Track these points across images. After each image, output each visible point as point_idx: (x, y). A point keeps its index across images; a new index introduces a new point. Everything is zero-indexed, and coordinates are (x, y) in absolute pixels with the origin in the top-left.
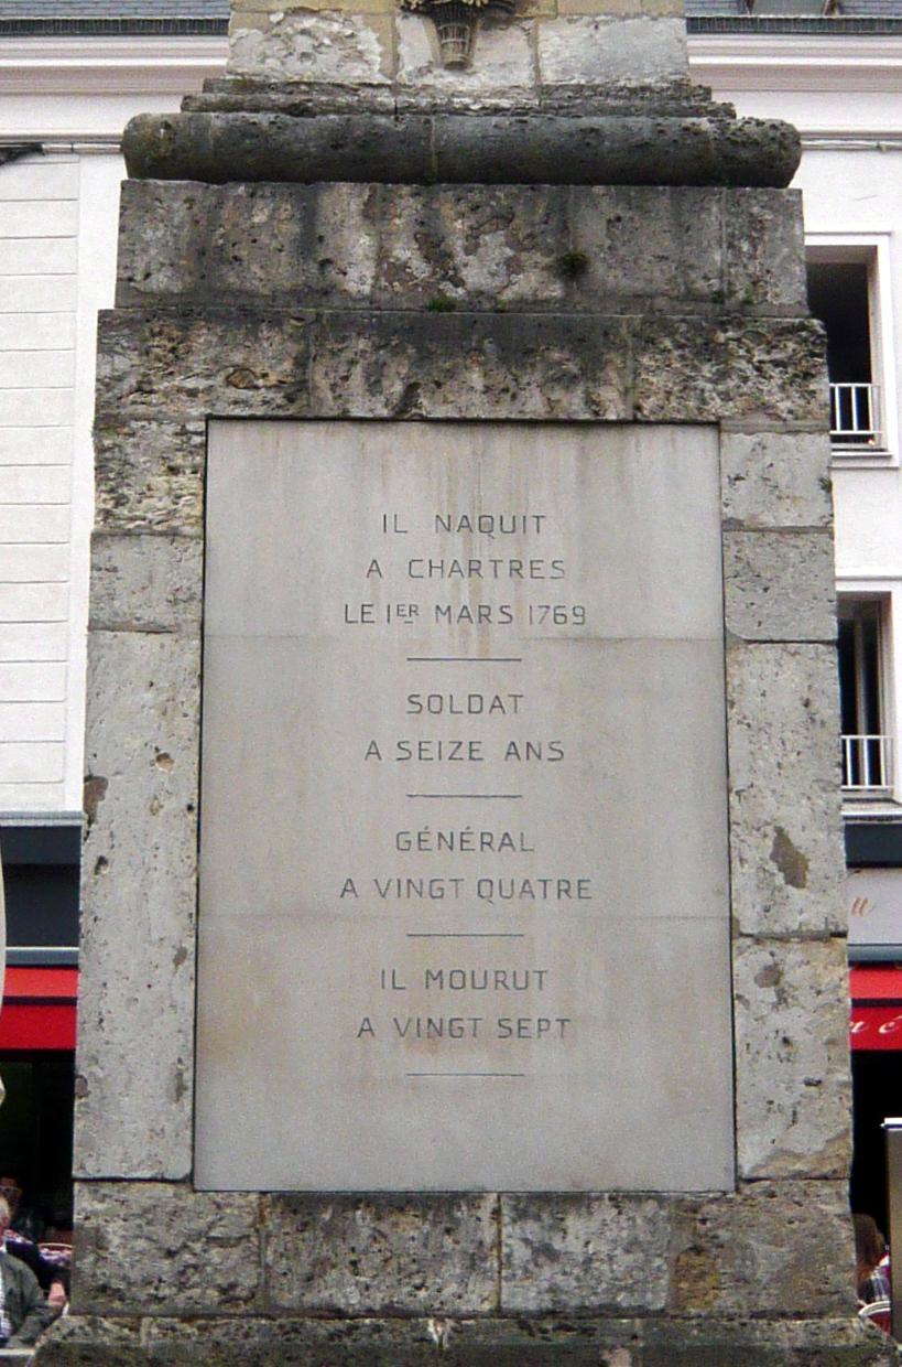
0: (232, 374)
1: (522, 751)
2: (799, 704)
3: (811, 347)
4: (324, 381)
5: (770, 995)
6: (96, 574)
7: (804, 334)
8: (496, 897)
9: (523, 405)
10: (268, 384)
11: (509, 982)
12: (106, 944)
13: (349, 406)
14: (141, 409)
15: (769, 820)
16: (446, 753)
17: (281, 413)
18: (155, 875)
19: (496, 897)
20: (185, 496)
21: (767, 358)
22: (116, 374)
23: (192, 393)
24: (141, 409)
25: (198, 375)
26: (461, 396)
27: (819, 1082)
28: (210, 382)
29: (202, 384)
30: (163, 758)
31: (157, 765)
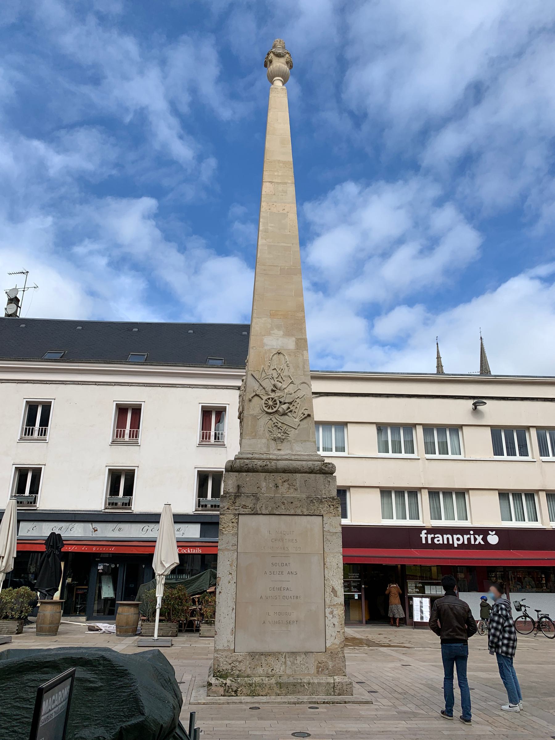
5: (331, 616)
7: (337, 500)
8: (286, 599)
11: (288, 614)
14: (227, 513)
16: (278, 574)
23: (236, 510)
24: (227, 513)
28: (239, 508)
29: (238, 508)
30: (231, 574)
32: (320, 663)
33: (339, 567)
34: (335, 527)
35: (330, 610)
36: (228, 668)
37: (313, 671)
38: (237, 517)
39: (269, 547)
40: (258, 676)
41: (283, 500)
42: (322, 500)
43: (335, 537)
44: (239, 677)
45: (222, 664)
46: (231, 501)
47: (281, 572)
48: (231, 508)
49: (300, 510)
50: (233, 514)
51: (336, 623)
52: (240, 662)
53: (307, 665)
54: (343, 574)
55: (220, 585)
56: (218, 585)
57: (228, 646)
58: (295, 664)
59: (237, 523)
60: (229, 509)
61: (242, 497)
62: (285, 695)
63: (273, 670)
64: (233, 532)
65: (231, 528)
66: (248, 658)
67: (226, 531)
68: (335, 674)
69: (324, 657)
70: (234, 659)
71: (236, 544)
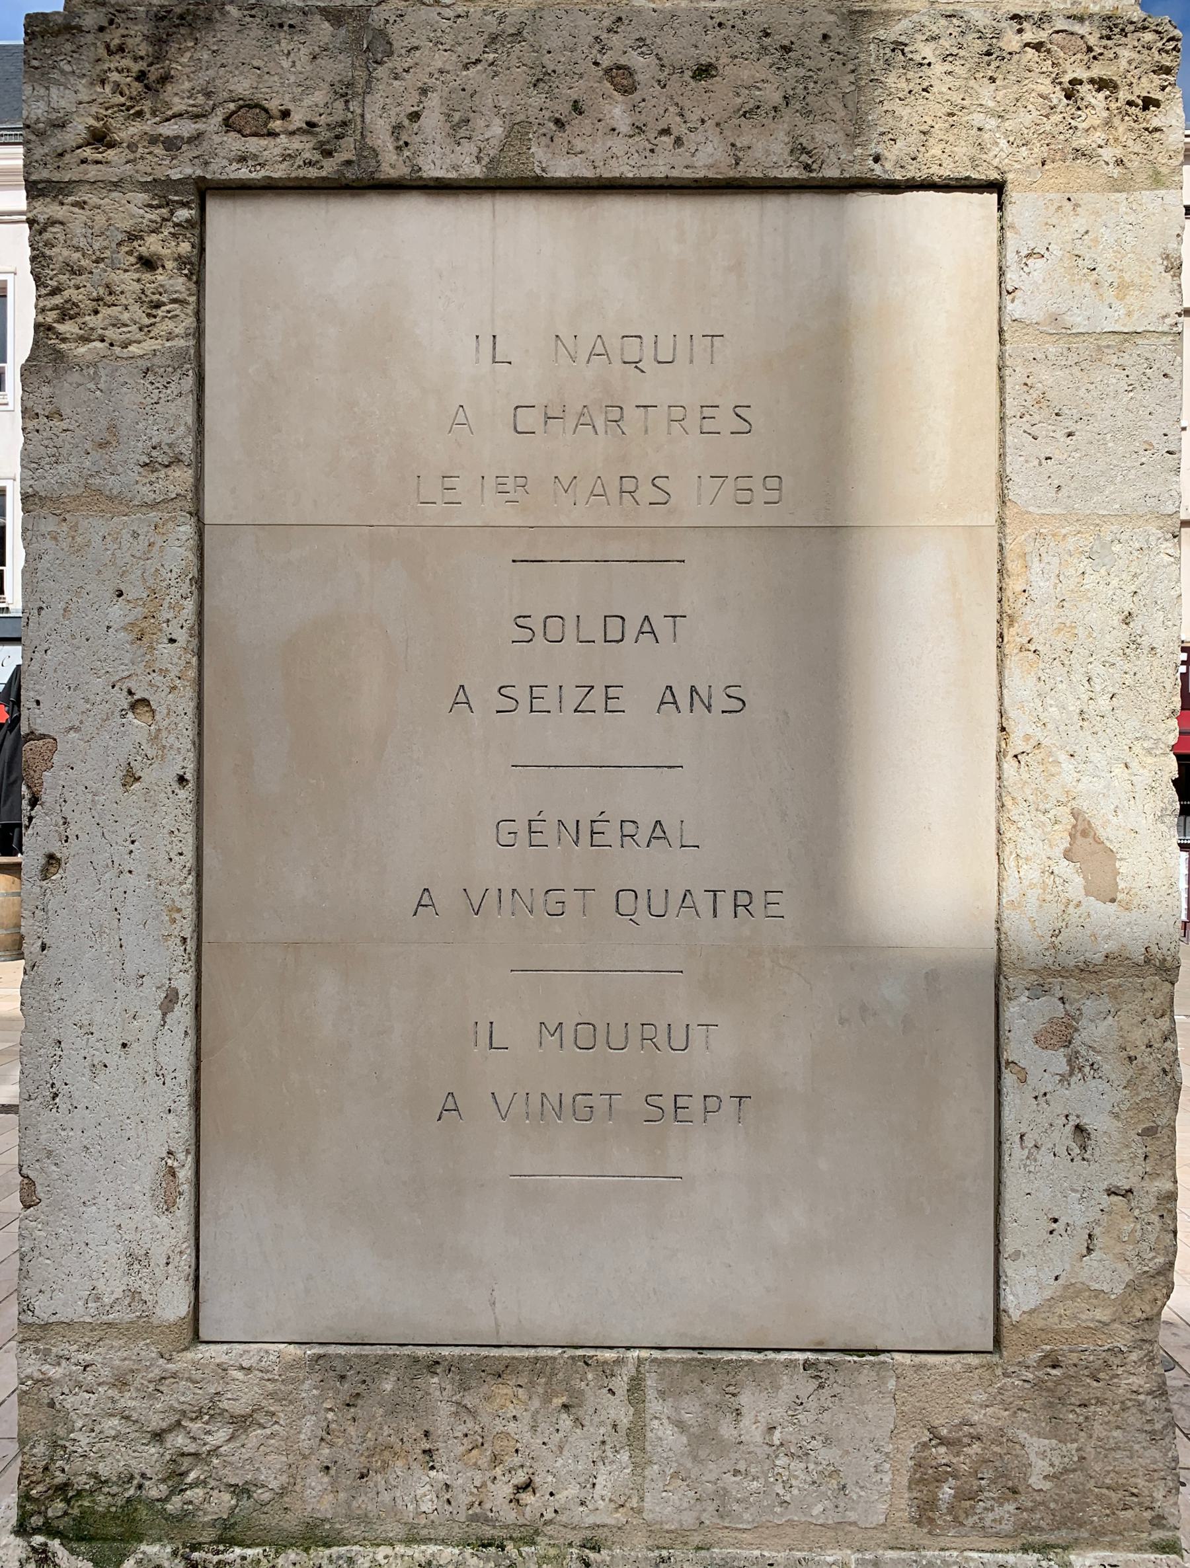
0: (234, 113)
1: (683, 700)
2: (1116, 620)
3: (1157, 57)
4: (381, 122)
5: (1058, 1061)
6: (31, 425)
7: (1148, 37)
8: (642, 916)
9: (693, 155)
10: (292, 128)
11: (661, 1040)
12: (59, 983)
13: (420, 161)
14: (93, 172)
15: (1064, 799)
16: (570, 702)
17: (312, 173)
18: (130, 881)
19: (642, 916)
20: (164, 304)
21: (1084, 75)
22: (54, 116)
23: (172, 144)
24: (93, 172)
25: (181, 115)
26: (594, 142)
27: (1130, 1191)
28: (200, 126)
29: (186, 128)
30: (139, 704)
31: (130, 715)
32: (943, 1441)
33: (1145, 641)
34: (1122, 288)
35: (1047, 1008)
36: (137, 1467)
37: (883, 1507)
38: (183, 214)
39: (490, 482)
40: (393, 1529)
41: (619, 50)
42: (998, 35)
43: (1115, 380)
44: (232, 1542)
45: (84, 1439)
46: (126, 65)
47: (597, 696)
48: (128, 131)
49: (782, 136)
50: (144, 186)
51: (1098, 1122)
52: (242, 1423)
53: (826, 1455)
54: (1177, 703)
55: (44, 798)
56: (34, 802)
57: (134, 1294)
58: (722, 1448)
59: (195, 267)
60: (111, 145)
61: (225, 30)
62: (1176, 540)
63: (527, 1486)
64: (149, 345)
65: (138, 313)
66: (308, 1390)
67: (86, 340)
68: (1084, 1534)
69: (979, 1397)
70: (182, 1395)
71: (186, 447)
